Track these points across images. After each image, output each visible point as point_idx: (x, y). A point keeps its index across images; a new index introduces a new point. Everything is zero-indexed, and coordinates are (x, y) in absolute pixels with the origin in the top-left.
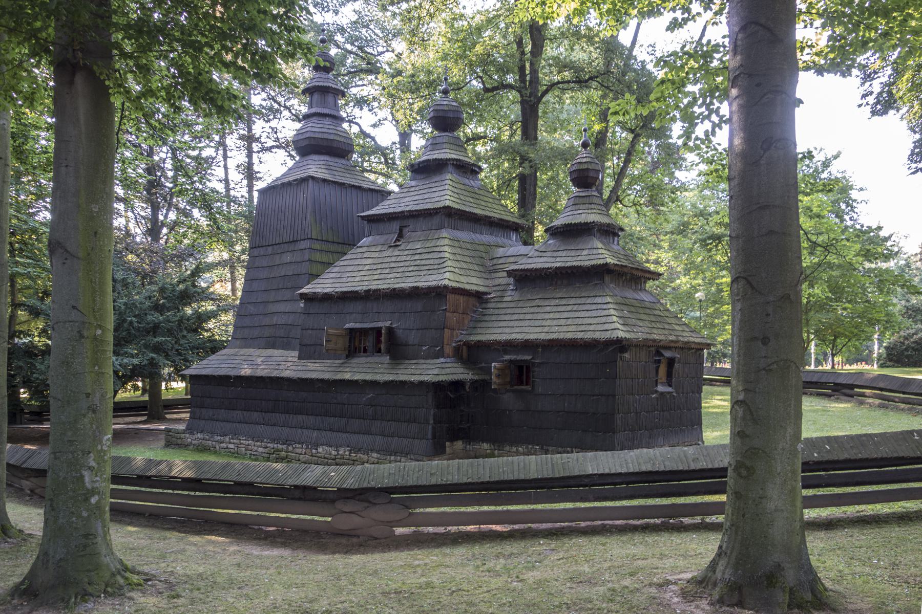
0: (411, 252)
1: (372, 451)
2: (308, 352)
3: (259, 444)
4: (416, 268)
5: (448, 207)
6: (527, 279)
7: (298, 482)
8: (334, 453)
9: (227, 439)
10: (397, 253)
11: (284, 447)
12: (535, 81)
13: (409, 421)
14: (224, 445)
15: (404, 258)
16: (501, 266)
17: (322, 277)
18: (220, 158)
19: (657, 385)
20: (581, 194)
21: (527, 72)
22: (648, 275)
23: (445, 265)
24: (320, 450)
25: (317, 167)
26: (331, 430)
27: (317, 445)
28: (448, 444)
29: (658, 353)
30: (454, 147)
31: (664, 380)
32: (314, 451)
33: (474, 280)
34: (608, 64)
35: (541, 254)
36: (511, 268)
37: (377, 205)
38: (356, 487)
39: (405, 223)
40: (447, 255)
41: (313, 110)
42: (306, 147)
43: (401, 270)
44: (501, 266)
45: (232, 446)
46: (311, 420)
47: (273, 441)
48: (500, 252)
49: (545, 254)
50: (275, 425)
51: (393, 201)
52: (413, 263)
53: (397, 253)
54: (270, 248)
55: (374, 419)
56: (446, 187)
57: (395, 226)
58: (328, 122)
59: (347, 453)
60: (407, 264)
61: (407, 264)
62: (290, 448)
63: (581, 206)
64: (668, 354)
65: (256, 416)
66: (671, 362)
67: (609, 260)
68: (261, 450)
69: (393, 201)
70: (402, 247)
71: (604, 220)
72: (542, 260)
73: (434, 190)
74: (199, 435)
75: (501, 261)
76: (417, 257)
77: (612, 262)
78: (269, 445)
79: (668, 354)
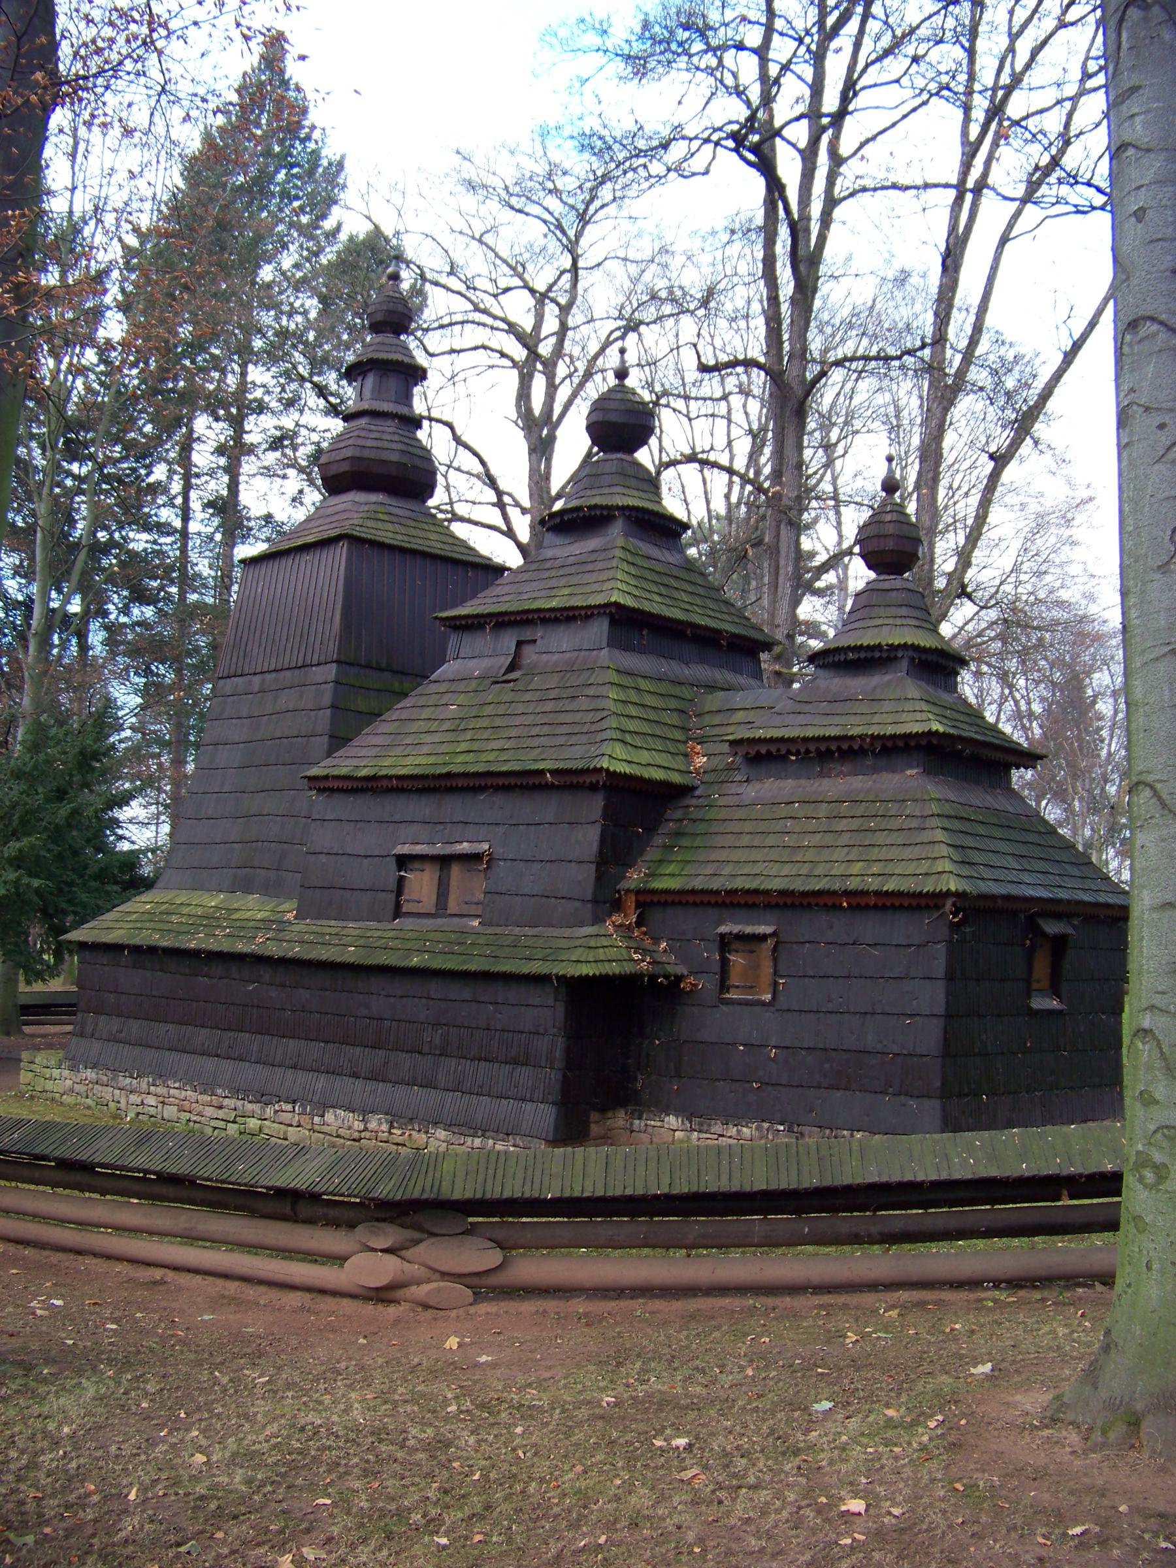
0: (537, 696)
1: (436, 1124)
2: (322, 899)
3: (207, 1098)
4: (546, 730)
5: (616, 604)
6: (764, 756)
7: (280, 1183)
8: (358, 1125)
9: (144, 1086)
10: (510, 696)
11: (256, 1107)
12: (801, 353)
13: (515, 1062)
14: (134, 1098)
15: (521, 708)
16: (715, 731)
17: (355, 743)
18: (176, 487)
19: (1029, 997)
20: (886, 585)
21: (786, 337)
22: (1011, 758)
23: (604, 724)
24: (329, 1117)
25: (358, 509)
26: (355, 1075)
27: (322, 1107)
28: (594, 1116)
29: (1032, 926)
30: (634, 483)
31: (1045, 983)
32: (317, 1119)
33: (661, 759)
34: (748, 103)
35: (798, 707)
36: (738, 736)
37: (474, 596)
38: (398, 1197)
39: (527, 634)
40: (610, 705)
41: (365, 406)
42: (340, 475)
43: (513, 733)
44: (715, 731)
45: (151, 1100)
46: (314, 1051)
47: (236, 1092)
48: (716, 700)
49: (807, 708)
50: (241, 1059)
51: (506, 589)
52: (539, 719)
53: (510, 696)
54: (257, 680)
55: (443, 1054)
56: (614, 563)
57: (508, 641)
58: (390, 426)
59: (385, 1127)
60: (528, 720)
61: (528, 720)
62: (269, 1111)
63: (882, 611)
64: (1052, 928)
65: (202, 1036)
66: (1059, 944)
67: (936, 726)
68: (209, 1112)
69: (506, 589)
70: (520, 685)
71: (924, 640)
72: (801, 719)
73: (590, 567)
74: (90, 1074)
75: (717, 720)
76: (549, 706)
77: (941, 729)
78: (226, 1102)
79: (1052, 928)
